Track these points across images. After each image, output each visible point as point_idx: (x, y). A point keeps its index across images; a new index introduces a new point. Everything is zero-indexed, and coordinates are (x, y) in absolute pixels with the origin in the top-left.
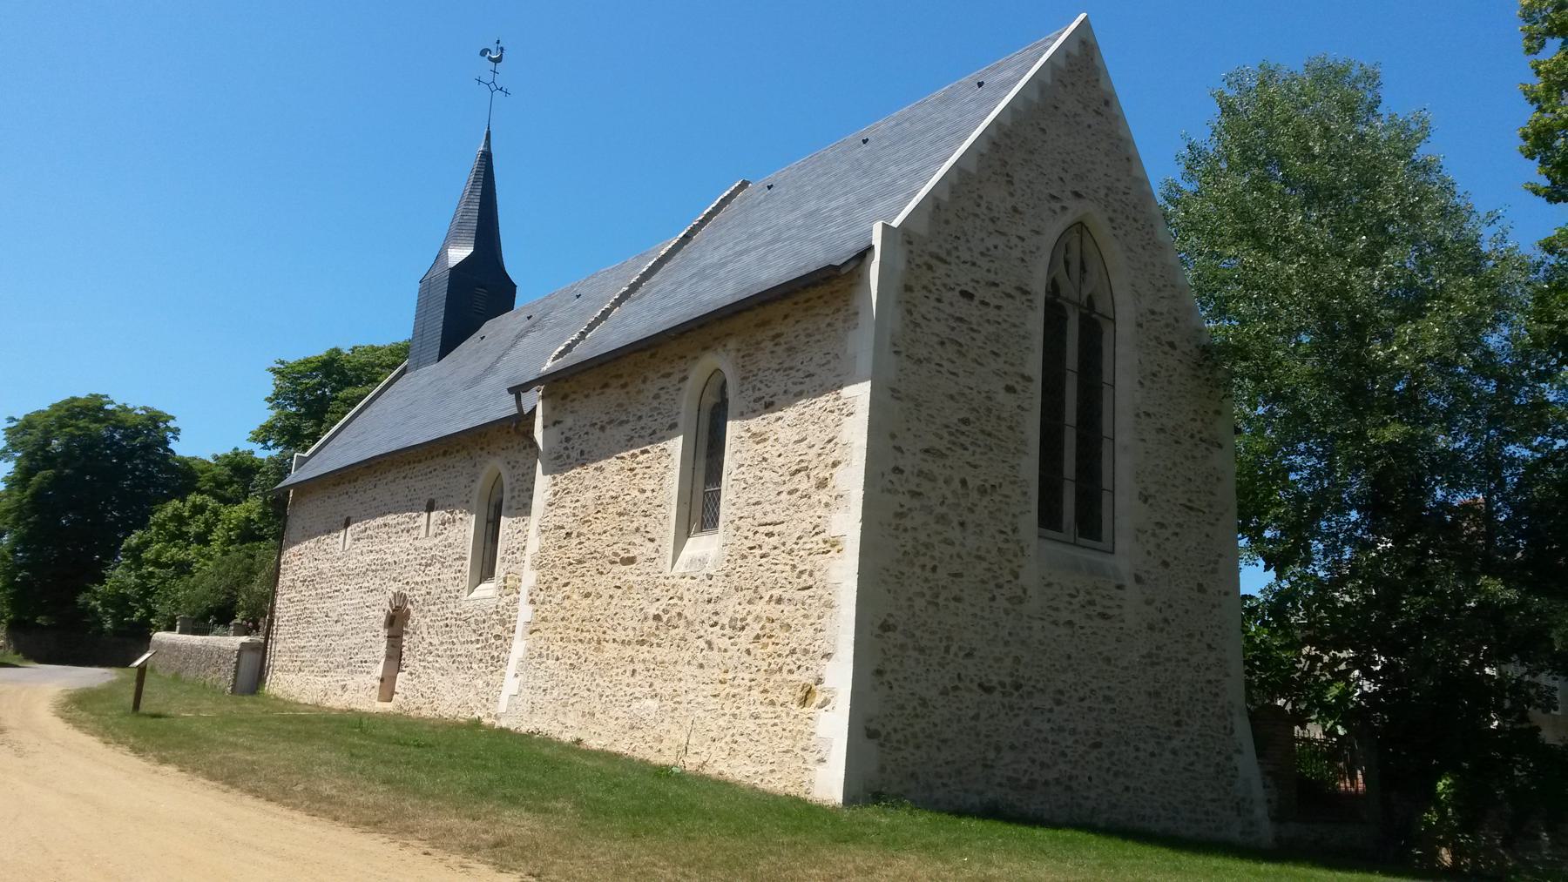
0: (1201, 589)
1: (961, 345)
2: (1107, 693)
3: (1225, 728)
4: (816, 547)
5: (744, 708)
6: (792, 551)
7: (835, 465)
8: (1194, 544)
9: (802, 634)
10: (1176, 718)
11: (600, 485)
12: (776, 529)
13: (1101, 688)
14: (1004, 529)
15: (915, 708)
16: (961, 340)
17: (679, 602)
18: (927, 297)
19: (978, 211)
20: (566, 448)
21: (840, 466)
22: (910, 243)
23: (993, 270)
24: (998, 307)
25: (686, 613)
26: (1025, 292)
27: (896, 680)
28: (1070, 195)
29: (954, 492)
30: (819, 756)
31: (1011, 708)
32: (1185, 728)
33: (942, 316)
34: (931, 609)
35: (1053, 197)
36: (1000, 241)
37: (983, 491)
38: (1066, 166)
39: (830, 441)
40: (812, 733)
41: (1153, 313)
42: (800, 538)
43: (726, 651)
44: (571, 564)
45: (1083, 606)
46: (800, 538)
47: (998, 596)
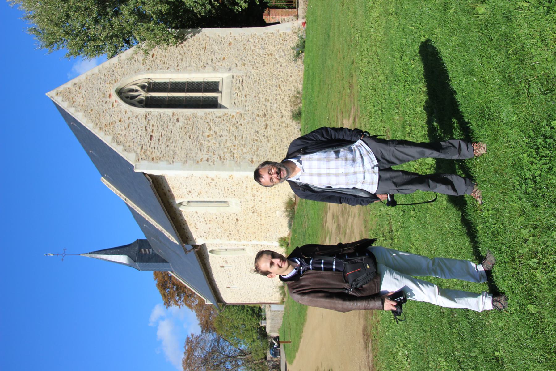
0: (230, 44)
1: (167, 139)
2: (265, 82)
3: (272, 36)
8: (217, 46)
10: (270, 56)
16: (165, 139)
19: (123, 135)
22: (139, 160)
24: (153, 126)
25: (252, 206)
26: (146, 116)
28: (110, 99)
29: (212, 139)
31: (271, 117)
32: (273, 53)
33: (159, 147)
34: (246, 146)
35: (113, 106)
37: (210, 130)
38: (101, 101)
45: (240, 91)
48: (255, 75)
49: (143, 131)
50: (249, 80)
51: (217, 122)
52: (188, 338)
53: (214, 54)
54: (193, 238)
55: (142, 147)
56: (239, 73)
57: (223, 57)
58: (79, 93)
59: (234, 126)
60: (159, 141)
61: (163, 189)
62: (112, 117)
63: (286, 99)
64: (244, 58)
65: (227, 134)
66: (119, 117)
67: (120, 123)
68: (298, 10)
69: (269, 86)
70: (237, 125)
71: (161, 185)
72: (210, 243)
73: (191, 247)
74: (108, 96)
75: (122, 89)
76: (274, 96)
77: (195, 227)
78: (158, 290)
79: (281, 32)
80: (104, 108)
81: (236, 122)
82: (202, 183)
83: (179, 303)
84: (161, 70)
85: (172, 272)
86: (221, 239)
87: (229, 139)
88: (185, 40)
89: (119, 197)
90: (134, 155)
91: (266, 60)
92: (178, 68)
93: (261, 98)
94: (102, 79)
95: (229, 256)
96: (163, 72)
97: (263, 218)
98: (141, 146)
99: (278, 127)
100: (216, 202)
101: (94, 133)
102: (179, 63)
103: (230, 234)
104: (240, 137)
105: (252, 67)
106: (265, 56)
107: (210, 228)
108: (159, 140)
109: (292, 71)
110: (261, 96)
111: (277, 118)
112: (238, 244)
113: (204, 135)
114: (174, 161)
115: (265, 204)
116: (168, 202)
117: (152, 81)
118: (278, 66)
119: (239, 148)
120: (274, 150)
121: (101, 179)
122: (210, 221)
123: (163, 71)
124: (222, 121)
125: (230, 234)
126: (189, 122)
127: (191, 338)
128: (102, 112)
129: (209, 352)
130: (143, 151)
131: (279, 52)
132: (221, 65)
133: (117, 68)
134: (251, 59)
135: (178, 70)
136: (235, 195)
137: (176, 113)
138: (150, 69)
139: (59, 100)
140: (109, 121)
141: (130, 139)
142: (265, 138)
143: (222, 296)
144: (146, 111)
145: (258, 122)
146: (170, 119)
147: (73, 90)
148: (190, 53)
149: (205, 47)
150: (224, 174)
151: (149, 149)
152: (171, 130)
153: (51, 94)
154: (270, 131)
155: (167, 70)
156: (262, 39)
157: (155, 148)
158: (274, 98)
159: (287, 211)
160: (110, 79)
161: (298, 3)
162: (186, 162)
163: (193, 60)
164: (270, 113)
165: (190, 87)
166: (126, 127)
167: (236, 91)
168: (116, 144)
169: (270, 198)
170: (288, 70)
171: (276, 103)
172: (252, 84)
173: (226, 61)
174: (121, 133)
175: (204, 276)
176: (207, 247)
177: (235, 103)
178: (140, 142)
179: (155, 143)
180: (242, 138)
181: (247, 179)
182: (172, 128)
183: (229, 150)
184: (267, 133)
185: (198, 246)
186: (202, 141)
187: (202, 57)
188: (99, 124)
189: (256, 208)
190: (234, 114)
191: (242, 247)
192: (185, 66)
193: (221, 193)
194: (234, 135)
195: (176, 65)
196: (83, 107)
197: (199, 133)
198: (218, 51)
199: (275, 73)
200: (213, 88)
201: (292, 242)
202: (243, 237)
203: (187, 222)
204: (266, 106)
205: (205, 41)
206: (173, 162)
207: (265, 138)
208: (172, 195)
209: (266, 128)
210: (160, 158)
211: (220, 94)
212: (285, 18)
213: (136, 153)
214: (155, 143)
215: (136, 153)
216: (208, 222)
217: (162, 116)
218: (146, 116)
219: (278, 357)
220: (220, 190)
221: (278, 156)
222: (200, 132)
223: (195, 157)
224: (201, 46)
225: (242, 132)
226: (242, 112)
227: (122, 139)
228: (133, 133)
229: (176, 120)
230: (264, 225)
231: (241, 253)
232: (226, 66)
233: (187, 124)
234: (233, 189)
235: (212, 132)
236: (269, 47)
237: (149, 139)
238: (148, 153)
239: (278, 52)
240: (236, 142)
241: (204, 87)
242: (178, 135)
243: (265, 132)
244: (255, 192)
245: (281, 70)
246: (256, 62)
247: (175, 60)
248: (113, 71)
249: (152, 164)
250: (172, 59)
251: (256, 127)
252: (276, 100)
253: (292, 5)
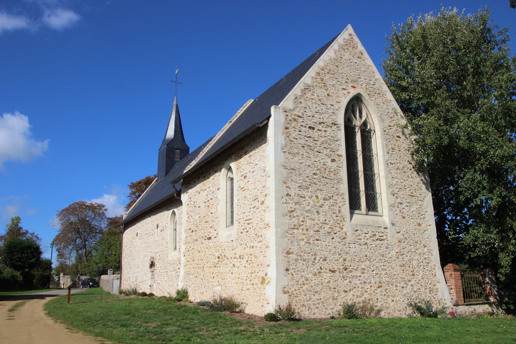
0: (419, 225)
1: (311, 146)
2: (383, 267)
3: (432, 274)
4: (262, 226)
5: (245, 286)
6: (255, 229)
7: (266, 196)
8: (415, 209)
9: (260, 259)
10: (412, 273)
11: (200, 213)
12: (251, 221)
13: (380, 266)
14: (336, 212)
15: (303, 282)
16: (311, 145)
17: (224, 251)
18: (295, 131)
19: (313, 97)
20: (190, 201)
21: (267, 196)
22: (286, 112)
23: (321, 118)
24: (325, 131)
25: (227, 255)
26: (335, 124)
27: (295, 272)
28: (351, 87)
29: (314, 201)
30: (267, 302)
31: (344, 277)
32: (416, 276)
33: (301, 137)
34: (307, 245)
35: (344, 89)
36: (324, 107)
37: (325, 199)
38: (348, 77)
39: (264, 187)
40: (265, 294)
41: (390, 126)
42: (257, 224)
43: (239, 267)
44: (194, 241)
45: (371, 237)
46: (257, 224)
47: (335, 237)
48: (390, 255)
49: (318, 119)
50: (383, 248)
51: (335, 208)
52: (103, 206)
53: (407, 206)
54: (189, 190)
55: (301, 117)
56: (391, 235)
57: (405, 216)
58: (353, 56)
59: (330, 230)
60: (308, 137)
61: (248, 145)
62: (332, 87)
63: (366, 296)
64: (407, 241)
65: (321, 221)
66: (332, 94)
67: (326, 94)
68: (464, 305)
69: (379, 273)
70: (332, 233)
71: (254, 141)
72: (182, 211)
73: (178, 190)
74: (354, 85)
75: (362, 101)
76: (369, 281)
77: (202, 190)
78: (145, 178)
79: (438, 285)
80: (340, 79)
81: (335, 231)
82: (258, 190)
83: (132, 196)
84: (385, 145)
85: (156, 181)
86: (187, 221)
87: (315, 222)
88: (418, 173)
89: (234, 116)
90: (291, 107)
91: (408, 268)
92: (389, 164)
93: (364, 264)
94: (370, 82)
95: (169, 233)
96: (383, 147)
97: (211, 270)
98: (302, 116)
99: (332, 287)
100: (232, 212)
101: (313, 66)
102: (394, 165)
103: (192, 231)
104: (318, 238)
105: (398, 251)
106: (411, 267)
107: (199, 207)
108: (310, 137)
109: (399, 302)
110: (368, 263)
111: (343, 284)
112: (181, 242)
113: (318, 191)
114: (286, 154)
115: (230, 272)
116: (232, 154)
117: (372, 135)
118: (402, 284)
119: (304, 236)
120: (304, 282)
122: (208, 206)
123: (385, 147)
124: (335, 215)
125: (192, 231)
126: (332, 174)
127: (103, 209)
128: (337, 77)
129: (90, 224)
130: (296, 118)
131: (417, 285)
132: (397, 214)
133: (382, 98)
134: (406, 250)
135: (387, 164)
136: (242, 233)
137: (342, 158)
138: (385, 133)
139: (340, 40)
140: (327, 83)
141: (309, 104)
142: (318, 269)
143: (129, 229)
144: (341, 124)
145: (337, 260)
146: (334, 152)
147: (356, 51)
148: (406, 179)
149: (413, 196)
150: (271, 217)
151: (299, 125)
152: (322, 152)
153: (350, 29)
154: (327, 275)
155: (386, 151)
156: (428, 263)
157: (300, 131)
158: (366, 281)
159: (221, 300)
160: (370, 89)
161: (471, 305)
162: (285, 167)
163: (399, 181)
164: (349, 276)
165: (369, 177)
166: (322, 101)
167: (370, 232)
168: (303, 88)
169: (238, 278)
170: (399, 297)
171: (361, 283)
172: (380, 251)
173: (402, 220)
174: (315, 95)
175: (148, 207)
176: (178, 208)
177: (357, 230)
178: (307, 115)
179: (305, 132)
180: (317, 240)
181: (264, 247)
182: (324, 154)
183: (302, 223)
184: (325, 272)
185: (180, 196)
186: (310, 189)
187: (403, 192)
188: (323, 72)
189: (224, 260)
190: (344, 230)
191: (178, 247)
192: (392, 172)
193: (245, 215)
194: (320, 230)
195: (393, 162)
196: (339, 58)
197: (320, 185)
198: (411, 211)
199: (394, 280)
200: (370, 204)
201: (182, 307)
202: (188, 247)
203: (207, 180)
204: (356, 270)
205: (419, 196)
206: (284, 152)
207: (318, 269)
208: (240, 157)
209: (330, 270)
210: (288, 137)
211: (364, 213)
212: (453, 290)
213: (294, 110)
214: (305, 132)
215: (294, 110)
216: (207, 204)
217: (336, 142)
218: (335, 124)
219: (81, 287)
220: (247, 214)
221: (296, 289)
222: (321, 186)
223: (292, 180)
224: (413, 192)
225: (324, 239)
226: (348, 240)
227: (309, 95)
228: (316, 108)
229: (333, 158)
230: (203, 271)
231: (171, 246)
232: (396, 220)
233: (329, 171)
234: (250, 230)
235: (322, 201)
236: (421, 271)
237: (310, 125)
238: (294, 124)
239: (418, 283)
240: (311, 233)
241: (370, 194)
242: (317, 160)
243: (326, 269)
244: (246, 259)
245: (398, 288)
246: (403, 256)
247: (397, 161)
248: (379, 94)
249: (282, 127)
250: (398, 157)
251: (330, 257)
252: (365, 282)
253: (467, 298)
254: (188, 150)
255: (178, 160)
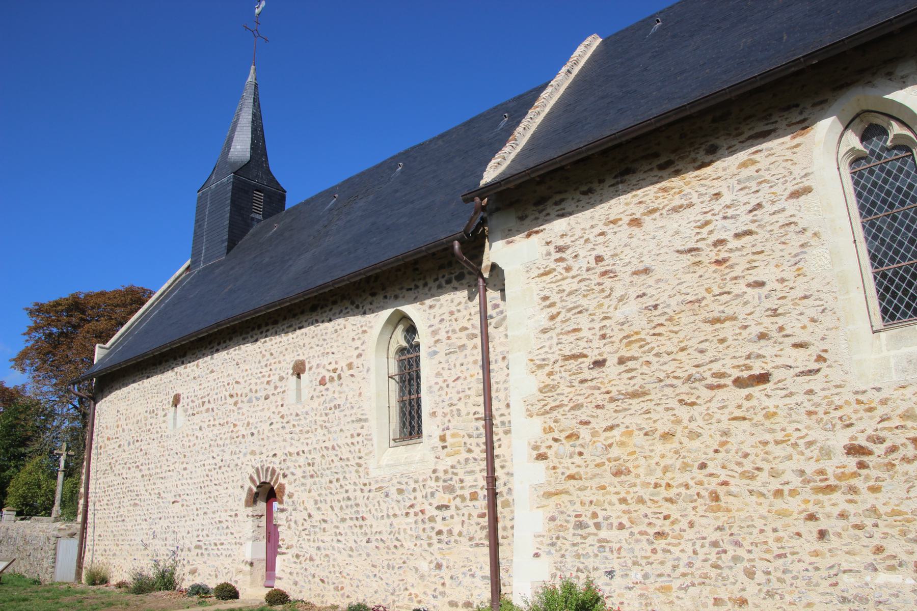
85: (188, 268)
121: (595, 35)
176: (428, 302)
254: (282, 198)
255: (260, 217)
